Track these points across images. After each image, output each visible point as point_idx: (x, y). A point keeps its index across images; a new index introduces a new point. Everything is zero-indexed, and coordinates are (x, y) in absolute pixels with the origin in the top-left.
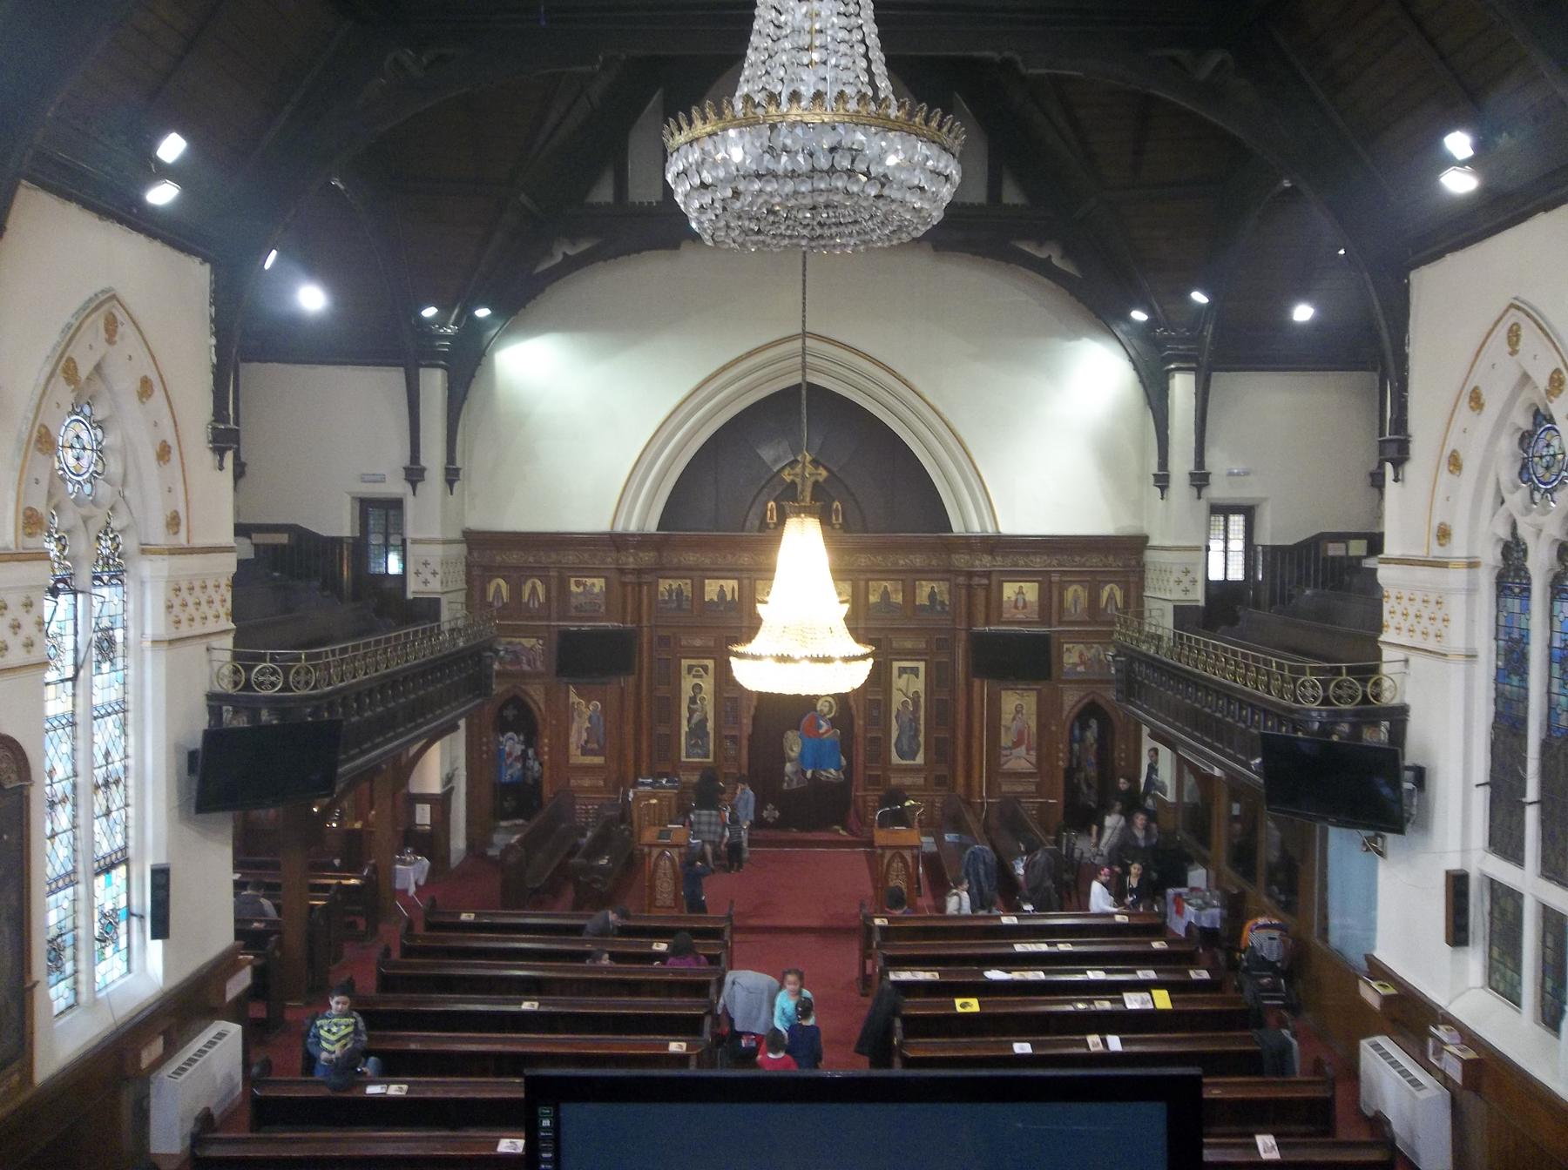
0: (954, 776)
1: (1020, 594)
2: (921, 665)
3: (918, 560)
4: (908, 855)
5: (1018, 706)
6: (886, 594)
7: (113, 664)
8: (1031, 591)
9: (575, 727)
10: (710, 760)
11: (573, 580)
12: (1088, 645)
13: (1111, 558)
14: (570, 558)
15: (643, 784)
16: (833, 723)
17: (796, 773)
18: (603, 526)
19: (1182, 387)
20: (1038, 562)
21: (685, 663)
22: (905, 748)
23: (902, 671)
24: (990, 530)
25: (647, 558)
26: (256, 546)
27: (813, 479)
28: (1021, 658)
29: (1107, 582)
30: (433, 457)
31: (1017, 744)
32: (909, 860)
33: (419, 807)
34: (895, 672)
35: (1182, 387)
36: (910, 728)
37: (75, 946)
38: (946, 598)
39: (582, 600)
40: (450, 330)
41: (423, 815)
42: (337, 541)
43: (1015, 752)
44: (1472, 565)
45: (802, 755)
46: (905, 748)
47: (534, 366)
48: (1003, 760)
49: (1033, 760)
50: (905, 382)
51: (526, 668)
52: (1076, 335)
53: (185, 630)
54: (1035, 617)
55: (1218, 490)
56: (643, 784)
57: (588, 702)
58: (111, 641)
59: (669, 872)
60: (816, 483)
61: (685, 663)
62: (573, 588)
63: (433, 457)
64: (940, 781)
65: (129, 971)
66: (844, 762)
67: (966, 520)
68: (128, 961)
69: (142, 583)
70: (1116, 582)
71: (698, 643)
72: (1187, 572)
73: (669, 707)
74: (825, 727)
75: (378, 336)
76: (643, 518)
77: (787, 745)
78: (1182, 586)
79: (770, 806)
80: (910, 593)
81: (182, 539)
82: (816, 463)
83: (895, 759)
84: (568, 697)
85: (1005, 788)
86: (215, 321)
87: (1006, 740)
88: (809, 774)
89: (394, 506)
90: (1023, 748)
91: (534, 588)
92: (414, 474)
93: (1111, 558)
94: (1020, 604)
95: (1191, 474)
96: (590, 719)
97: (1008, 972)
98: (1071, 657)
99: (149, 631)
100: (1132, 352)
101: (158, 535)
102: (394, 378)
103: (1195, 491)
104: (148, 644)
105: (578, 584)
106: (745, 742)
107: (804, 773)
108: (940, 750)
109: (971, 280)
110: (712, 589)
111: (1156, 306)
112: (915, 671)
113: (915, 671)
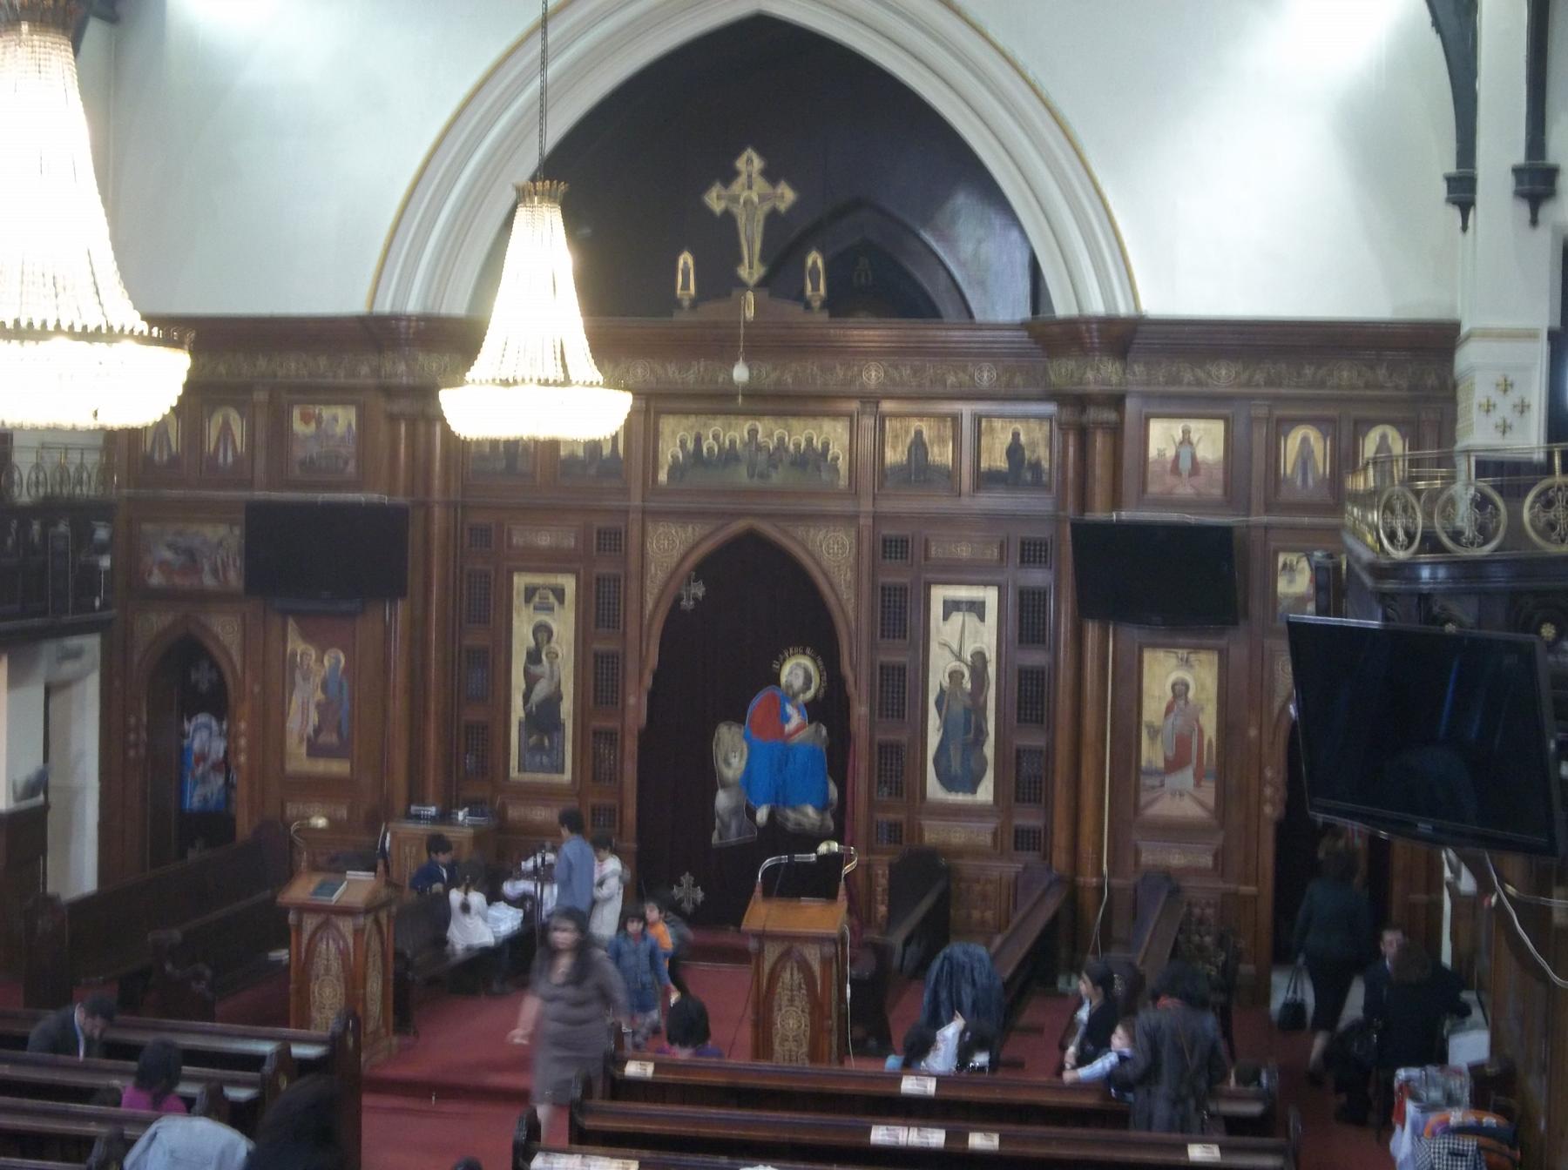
0: (1049, 829)
1: (1182, 446)
2: (990, 596)
4: (813, 955)
5: (1177, 682)
8: (1208, 439)
10: (567, 777)
11: (296, 413)
13: (1382, 373)
14: (293, 367)
15: (418, 817)
16: (814, 711)
17: (735, 811)
18: (353, 302)
20: (1223, 376)
21: (520, 581)
22: (956, 767)
23: (951, 607)
24: (1123, 309)
27: (766, 207)
28: (1161, 574)
29: (1373, 423)
31: (1175, 764)
32: (817, 968)
34: (937, 609)
36: (965, 729)
38: (1043, 453)
39: (314, 450)
45: (748, 772)
46: (956, 767)
51: (209, 581)
54: (1217, 492)
56: (418, 817)
57: (322, 651)
59: (335, 966)
60: (773, 218)
62: (298, 426)
64: (1025, 840)
71: (544, 540)
72: (1506, 386)
74: (795, 719)
77: (719, 753)
78: (1496, 417)
79: (687, 879)
83: (935, 790)
84: (285, 642)
85: (1147, 858)
87: (1152, 753)
88: (762, 815)
91: (226, 426)
93: (1382, 373)
94: (1185, 465)
95: (1517, 171)
96: (325, 687)
103: (1524, 210)
105: (306, 419)
106: (631, 745)
107: (751, 814)
108: (1025, 781)
112: (977, 608)
113: (977, 608)
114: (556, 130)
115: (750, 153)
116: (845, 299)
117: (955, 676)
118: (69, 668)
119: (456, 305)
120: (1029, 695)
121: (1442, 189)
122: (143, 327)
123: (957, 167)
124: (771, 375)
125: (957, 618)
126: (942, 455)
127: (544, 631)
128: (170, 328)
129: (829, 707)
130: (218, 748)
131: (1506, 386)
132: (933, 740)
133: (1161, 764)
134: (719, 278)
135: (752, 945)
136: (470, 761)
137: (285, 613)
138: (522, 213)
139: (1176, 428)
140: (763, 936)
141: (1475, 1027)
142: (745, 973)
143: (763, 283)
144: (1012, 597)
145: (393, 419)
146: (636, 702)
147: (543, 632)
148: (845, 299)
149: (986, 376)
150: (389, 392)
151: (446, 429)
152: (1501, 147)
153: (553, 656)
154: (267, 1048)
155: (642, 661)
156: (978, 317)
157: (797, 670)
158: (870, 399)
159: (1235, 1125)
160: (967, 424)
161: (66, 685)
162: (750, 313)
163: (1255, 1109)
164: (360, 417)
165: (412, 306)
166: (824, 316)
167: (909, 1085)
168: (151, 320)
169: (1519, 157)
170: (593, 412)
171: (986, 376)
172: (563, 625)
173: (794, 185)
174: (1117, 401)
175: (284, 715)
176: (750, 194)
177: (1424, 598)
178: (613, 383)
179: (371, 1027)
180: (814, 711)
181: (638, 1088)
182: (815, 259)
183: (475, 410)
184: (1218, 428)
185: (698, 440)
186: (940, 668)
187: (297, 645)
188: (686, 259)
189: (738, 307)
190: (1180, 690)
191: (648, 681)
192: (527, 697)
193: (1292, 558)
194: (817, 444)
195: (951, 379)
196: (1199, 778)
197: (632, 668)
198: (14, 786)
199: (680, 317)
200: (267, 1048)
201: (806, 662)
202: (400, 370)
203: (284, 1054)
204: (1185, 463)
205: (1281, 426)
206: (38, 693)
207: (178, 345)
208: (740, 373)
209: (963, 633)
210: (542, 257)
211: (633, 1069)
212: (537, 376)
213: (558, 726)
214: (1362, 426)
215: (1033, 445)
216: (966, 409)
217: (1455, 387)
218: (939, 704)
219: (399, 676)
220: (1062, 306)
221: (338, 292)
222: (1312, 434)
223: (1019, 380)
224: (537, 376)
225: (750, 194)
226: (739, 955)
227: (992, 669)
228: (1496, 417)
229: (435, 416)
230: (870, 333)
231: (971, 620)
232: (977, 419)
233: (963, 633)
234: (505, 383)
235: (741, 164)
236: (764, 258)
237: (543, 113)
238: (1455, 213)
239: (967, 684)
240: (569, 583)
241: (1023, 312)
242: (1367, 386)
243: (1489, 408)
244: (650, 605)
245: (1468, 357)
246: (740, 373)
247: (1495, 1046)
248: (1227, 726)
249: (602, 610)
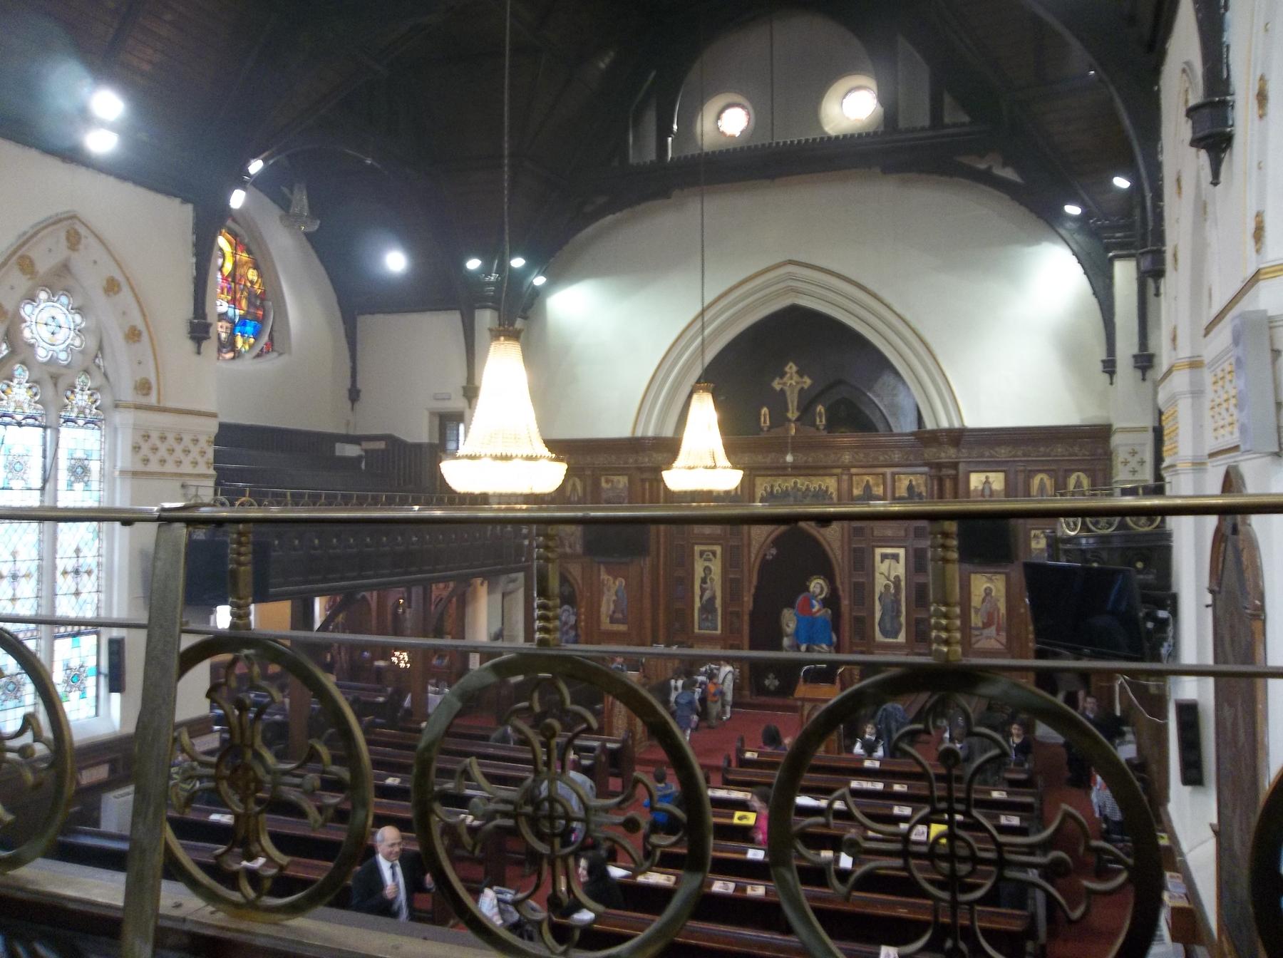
1: (985, 485)
2: (901, 552)
7: (86, 484)
8: (997, 481)
9: (605, 599)
10: (719, 632)
11: (603, 480)
13: (1076, 449)
14: (601, 460)
16: (826, 603)
20: (1003, 453)
21: (697, 548)
22: (888, 626)
23: (884, 557)
24: (957, 425)
26: (366, 451)
27: (799, 387)
31: (987, 625)
33: (472, 655)
34: (878, 558)
38: (923, 489)
40: (493, 277)
42: (418, 446)
43: (986, 632)
45: (797, 632)
46: (888, 626)
48: (974, 640)
49: (1004, 641)
50: (875, 296)
51: (568, 550)
52: (1035, 240)
53: (154, 467)
57: (615, 578)
58: (86, 470)
61: (697, 548)
62: (604, 485)
65: (97, 714)
66: (834, 638)
68: (97, 707)
69: (115, 430)
70: (1083, 471)
74: (817, 607)
78: (1129, 467)
81: (152, 400)
82: (800, 373)
83: (879, 637)
84: (599, 575)
86: (196, 245)
87: (976, 620)
90: (993, 629)
91: (574, 485)
93: (1076, 449)
94: (987, 492)
96: (616, 594)
97: (816, 799)
99: (119, 464)
100: (1075, 247)
101: (127, 394)
103: (1139, 374)
104: (117, 473)
105: (607, 481)
106: (746, 618)
109: (931, 201)
111: (1086, 198)
112: (895, 557)
113: (895, 557)
114: (710, 356)
115: (791, 364)
116: (834, 424)
117: (887, 587)
118: (511, 586)
119: (668, 432)
120: (919, 596)
121: (1100, 366)
122: (549, 454)
123: (883, 364)
124: (803, 459)
125: (887, 562)
127: (708, 568)
128: (559, 448)
129: (832, 601)
130: (572, 620)
131: (1134, 453)
132: (878, 615)
133: (980, 625)
134: (779, 419)
135: (799, 703)
136: (677, 625)
137: (599, 563)
138: (695, 397)
139: (982, 477)
140: (803, 700)
141: (1129, 742)
142: (797, 715)
143: (798, 419)
144: (911, 552)
145: (643, 481)
146: (748, 599)
148: (834, 424)
149: (897, 457)
150: (641, 470)
151: (665, 486)
152: (1126, 347)
153: (712, 580)
154: (596, 744)
155: (750, 582)
156: (895, 431)
157: (817, 585)
158: (847, 468)
159: (1013, 783)
160: (889, 477)
161: (511, 593)
162: (793, 432)
163: (1023, 776)
164: (630, 482)
165: (650, 433)
166: (825, 433)
167: (867, 764)
168: (551, 444)
169: (1136, 350)
170: (728, 479)
171: (897, 457)
172: (716, 567)
173: (810, 377)
174: (955, 465)
175: (599, 606)
176: (792, 381)
177: (1083, 552)
178: (735, 466)
179: (638, 737)
180: (826, 603)
181: (750, 763)
182: (820, 408)
183: (677, 479)
184: (1001, 476)
185: (772, 487)
186: (880, 583)
187: (604, 576)
188: (765, 410)
189: (788, 430)
190: (988, 592)
191: (753, 591)
192: (701, 598)
193: (1038, 532)
194: (824, 487)
195: (881, 458)
196: (998, 631)
197: (746, 584)
199: (763, 435)
200: (596, 744)
201: (821, 581)
202: (645, 460)
203: (603, 747)
204: (986, 490)
205: (1030, 474)
206: (498, 597)
207: (562, 461)
208: (789, 458)
209: (890, 567)
210: (703, 424)
211: (748, 755)
212: (703, 464)
213: (714, 610)
214: (1068, 472)
215: (918, 485)
216: (888, 471)
217: (1111, 453)
218: (880, 599)
219: (647, 590)
220: (929, 425)
221: (618, 427)
222: (1044, 476)
223: (912, 457)
224: (703, 464)
225: (792, 381)
226: (793, 709)
227: (903, 584)
228: (1129, 467)
229: (660, 480)
230: (846, 438)
231: (893, 562)
232: (893, 474)
233: (890, 567)
234: (690, 468)
235: (787, 369)
236: (798, 409)
237: (703, 352)
238: (1107, 376)
239: (892, 591)
240: (718, 549)
241: (914, 428)
242: (1070, 455)
243: (1126, 463)
244: (753, 556)
245: (1116, 440)
246: (789, 458)
247: (1139, 750)
249: (732, 560)
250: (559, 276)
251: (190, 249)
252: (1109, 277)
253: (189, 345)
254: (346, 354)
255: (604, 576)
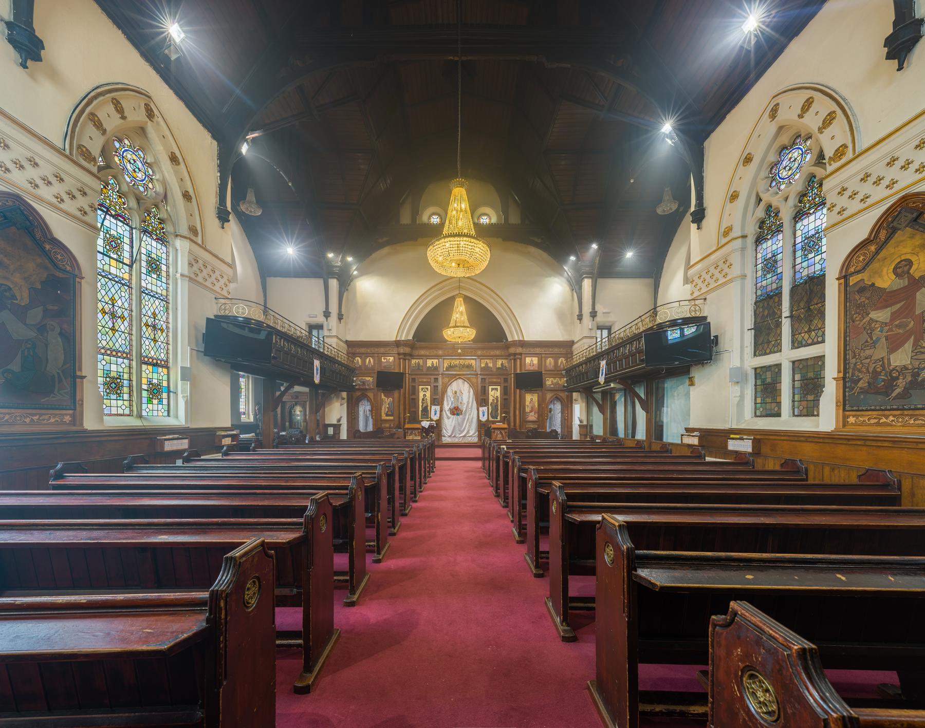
1: (531, 362)
3: (498, 352)
6: (487, 364)
8: (536, 360)
12: (554, 378)
14: (382, 350)
19: (587, 284)
20: (538, 350)
23: (493, 389)
25: (407, 350)
30: (334, 309)
35: (587, 284)
37: (130, 386)
41: (331, 431)
44: (744, 237)
47: (368, 286)
52: (550, 276)
55: (600, 318)
63: (334, 309)
67: (512, 336)
73: (415, 401)
75: (318, 270)
76: (407, 335)
80: (495, 364)
87: (527, 410)
89: (320, 327)
92: (327, 314)
98: (549, 382)
99: (179, 271)
102: (320, 282)
110: (429, 363)
112: (496, 389)
126: (491, 365)
147: (425, 395)
152: (587, 309)
172: (428, 394)
190: (532, 400)
198: (196, 328)
204: (532, 364)
219: (402, 402)
248: (539, 405)
250: (363, 272)
251: (216, 169)
252: (580, 288)
253: (217, 222)
254: (262, 294)
255: (383, 397)
